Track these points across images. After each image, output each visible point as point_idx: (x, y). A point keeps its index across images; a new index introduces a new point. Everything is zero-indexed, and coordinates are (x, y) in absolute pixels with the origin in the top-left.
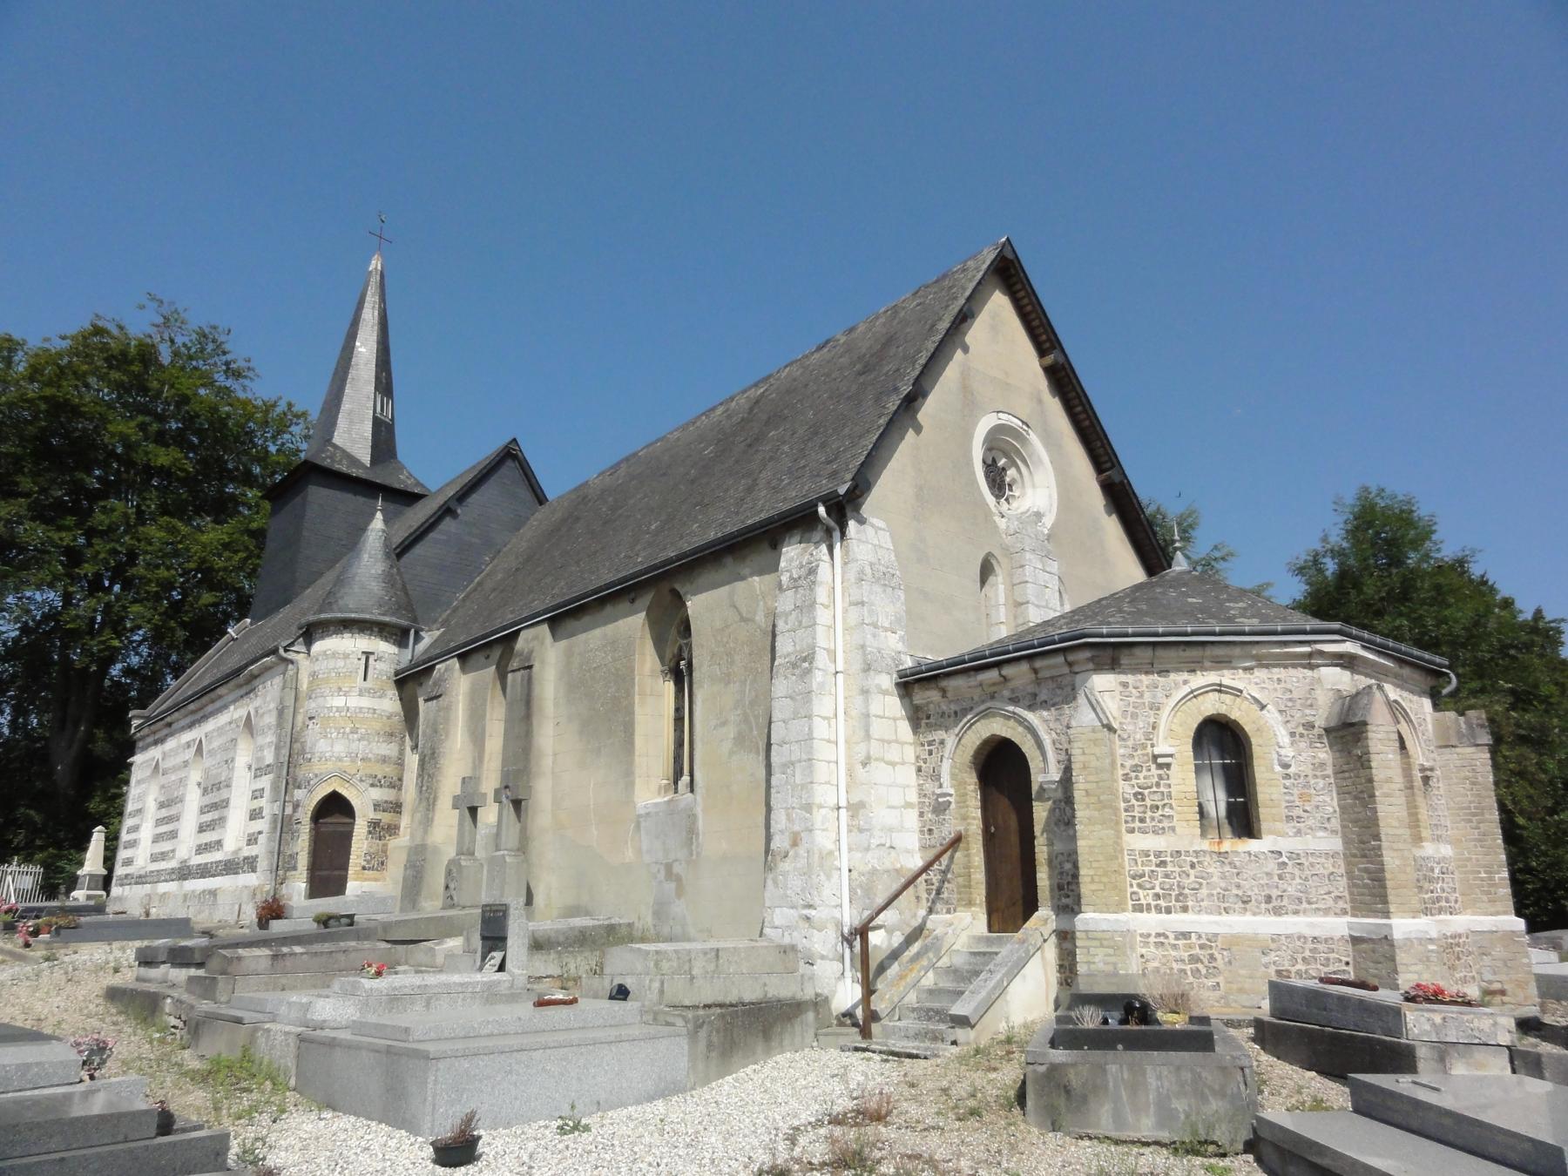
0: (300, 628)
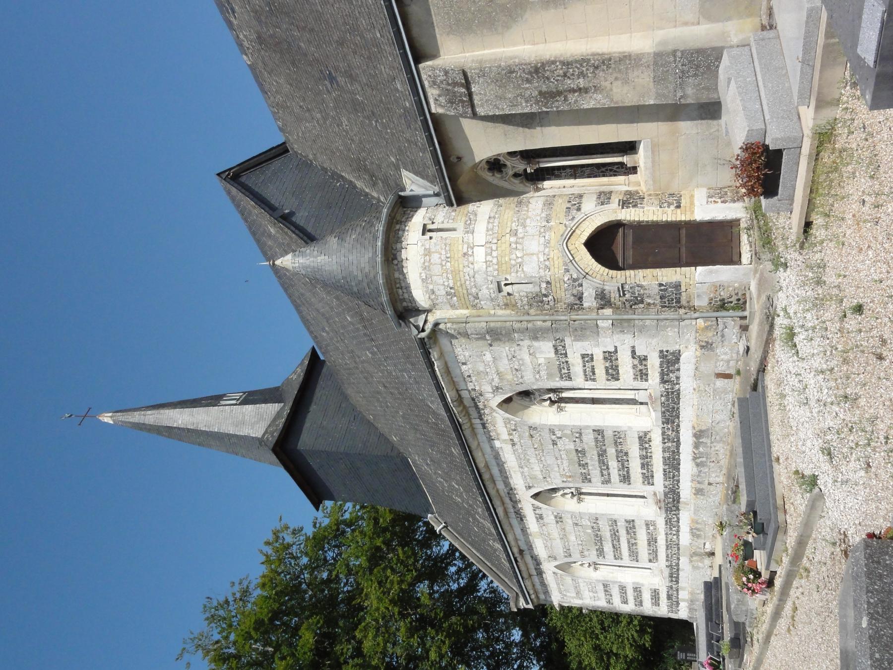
0: (400, 325)
